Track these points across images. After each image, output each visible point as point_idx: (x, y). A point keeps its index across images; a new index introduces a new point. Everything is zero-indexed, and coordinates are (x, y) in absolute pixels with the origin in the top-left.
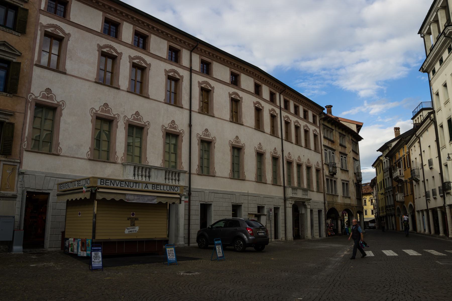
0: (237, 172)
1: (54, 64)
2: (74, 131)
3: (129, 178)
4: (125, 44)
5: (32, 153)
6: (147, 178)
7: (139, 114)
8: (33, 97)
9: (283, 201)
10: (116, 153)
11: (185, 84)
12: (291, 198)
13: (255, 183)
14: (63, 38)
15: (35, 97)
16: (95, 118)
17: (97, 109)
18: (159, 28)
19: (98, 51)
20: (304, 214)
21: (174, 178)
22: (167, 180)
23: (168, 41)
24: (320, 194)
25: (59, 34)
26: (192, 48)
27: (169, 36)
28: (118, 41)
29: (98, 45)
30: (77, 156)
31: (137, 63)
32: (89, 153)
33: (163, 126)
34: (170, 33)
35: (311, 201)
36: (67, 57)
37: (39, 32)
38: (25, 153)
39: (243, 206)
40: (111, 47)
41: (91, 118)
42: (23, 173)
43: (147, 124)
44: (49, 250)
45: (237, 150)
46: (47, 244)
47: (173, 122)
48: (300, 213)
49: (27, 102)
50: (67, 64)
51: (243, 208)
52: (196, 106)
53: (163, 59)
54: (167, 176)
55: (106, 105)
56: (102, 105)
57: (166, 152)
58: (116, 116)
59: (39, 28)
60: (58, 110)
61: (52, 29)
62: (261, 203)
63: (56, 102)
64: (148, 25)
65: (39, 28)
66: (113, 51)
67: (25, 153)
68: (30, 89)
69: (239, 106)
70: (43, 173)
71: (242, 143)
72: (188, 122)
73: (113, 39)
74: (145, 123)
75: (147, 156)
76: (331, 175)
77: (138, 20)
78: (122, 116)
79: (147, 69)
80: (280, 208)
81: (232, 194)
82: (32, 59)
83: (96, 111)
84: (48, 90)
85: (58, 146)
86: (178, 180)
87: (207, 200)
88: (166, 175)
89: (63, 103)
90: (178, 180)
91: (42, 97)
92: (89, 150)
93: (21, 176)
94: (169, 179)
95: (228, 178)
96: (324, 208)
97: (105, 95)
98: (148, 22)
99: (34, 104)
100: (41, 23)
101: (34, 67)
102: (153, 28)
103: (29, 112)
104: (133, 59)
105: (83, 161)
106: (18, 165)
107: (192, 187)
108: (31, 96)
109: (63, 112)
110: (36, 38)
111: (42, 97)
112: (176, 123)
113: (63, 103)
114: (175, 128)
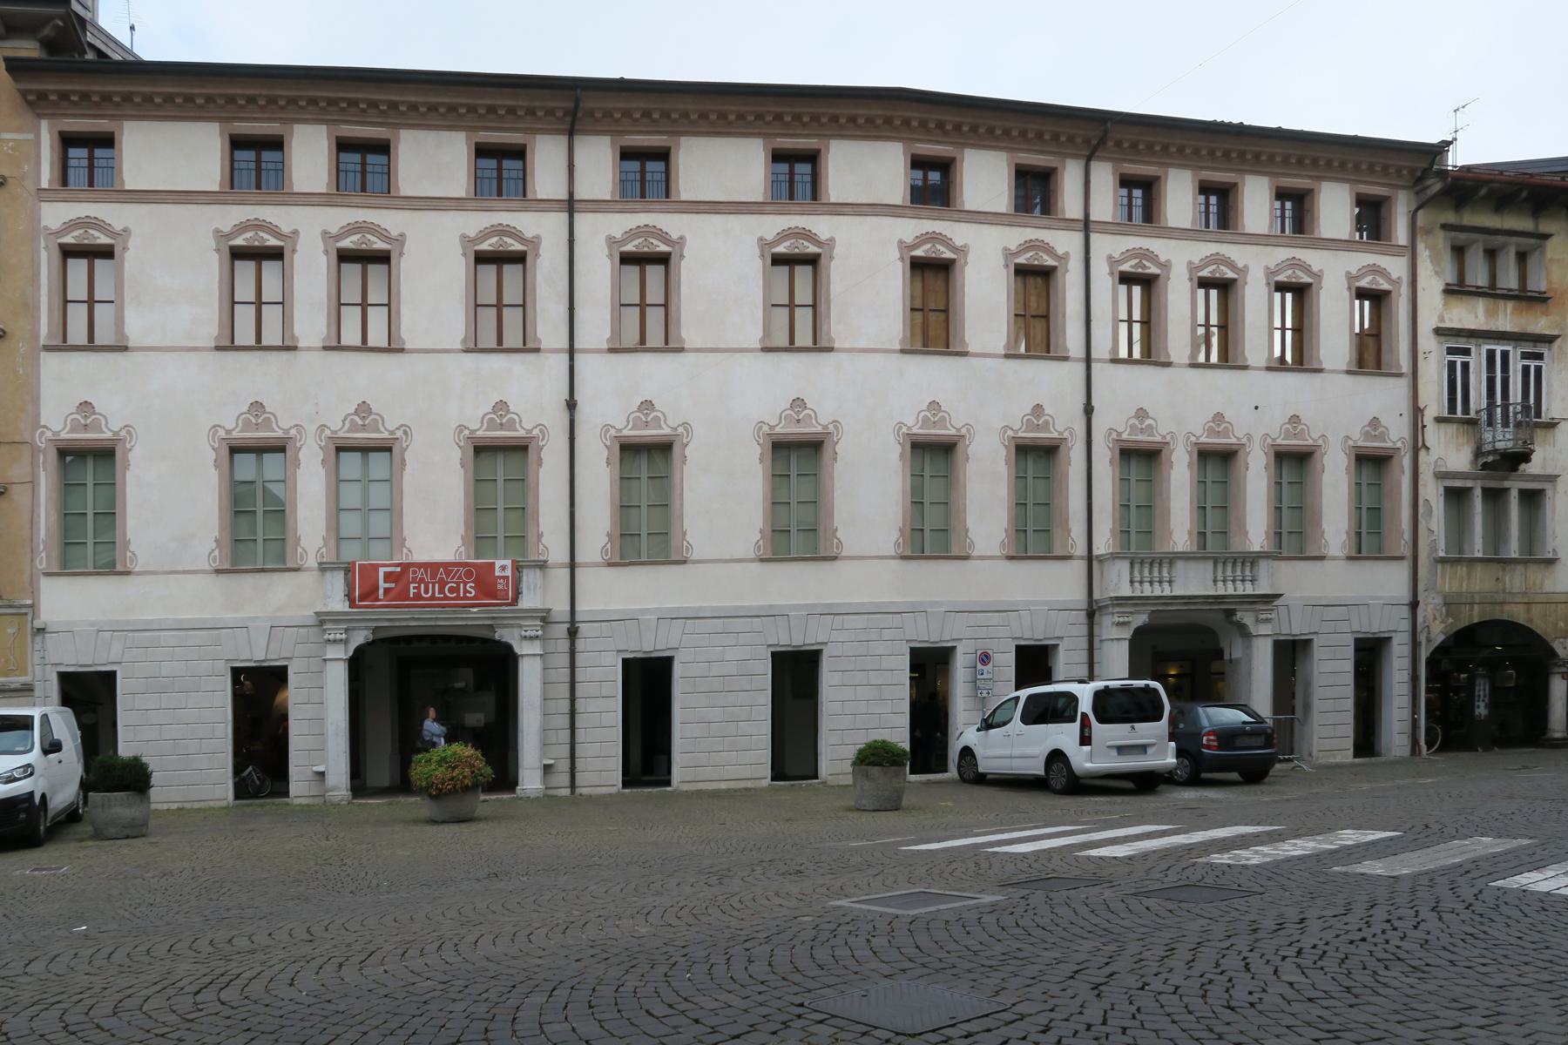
0: (931, 532)
1: (377, 337)
2: (172, 501)
3: (329, 609)
4: (308, 199)
5: (287, 574)
6: (1166, 585)
7: (369, 411)
8: (49, 434)
9: (1405, 612)
10: (684, 534)
11: (548, 266)
12: (1121, 601)
13: (893, 562)
14: (669, 254)
15: (55, 433)
16: (908, 447)
17: (230, 426)
18: (413, 99)
19: (218, 250)
20: (1238, 661)
21: (1137, 577)
22: (1220, 584)
23: (469, 129)
24: (1395, 564)
25: (99, 241)
26: (569, 119)
27: (463, 111)
28: (956, 216)
29: (217, 231)
30: (180, 568)
31: (352, 246)
32: (216, 553)
33: (461, 428)
34: (77, 87)
35: (1278, 602)
36: (127, 300)
37: (44, 255)
38: (45, 583)
39: (1315, 644)
40: (259, 225)
41: (213, 455)
42: (41, 631)
43: (399, 434)
44: (685, 787)
45: (934, 454)
46: (825, 768)
47: (501, 406)
48: (1227, 657)
49: (35, 451)
50: (127, 320)
51: (1318, 652)
52: (595, 325)
53: (453, 203)
54: (1137, 574)
55: (257, 407)
56: (245, 409)
57: (479, 510)
58: (293, 432)
59: (43, 244)
60: (676, 449)
61: (76, 233)
62: (930, 635)
63: (108, 435)
64: (373, 104)
65: (43, 244)
66: (266, 236)
67: (45, 583)
68: (37, 416)
69: (1052, 284)
70: (92, 624)
71: (391, 426)
72: (1082, 399)
73: (638, 206)
74: (392, 432)
75: (406, 533)
76: (1485, 466)
77: (332, 102)
78: (311, 429)
79: (1059, 273)
80: (1395, 642)
81: (770, 614)
82: (35, 335)
83: (228, 432)
84: (86, 406)
85: (684, 539)
86: (1170, 582)
87: (648, 645)
88: (1132, 573)
89: (129, 432)
90: (1170, 582)
91: (72, 431)
92: (214, 545)
93: (38, 639)
94: (1141, 582)
95: (752, 561)
96: (1405, 625)
97: (933, 378)
98: (447, 100)
99: (52, 455)
100: (46, 228)
101: (43, 354)
102: (394, 106)
103: (43, 475)
104: (338, 237)
105: (199, 576)
106: (29, 611)
107: (578, 608)
108: (42, 433)
109: (132, 456)
110: (36, 276)
111: (72, 431)
112: (512, 409)
113: (129, 432)
114: (511, 425)
